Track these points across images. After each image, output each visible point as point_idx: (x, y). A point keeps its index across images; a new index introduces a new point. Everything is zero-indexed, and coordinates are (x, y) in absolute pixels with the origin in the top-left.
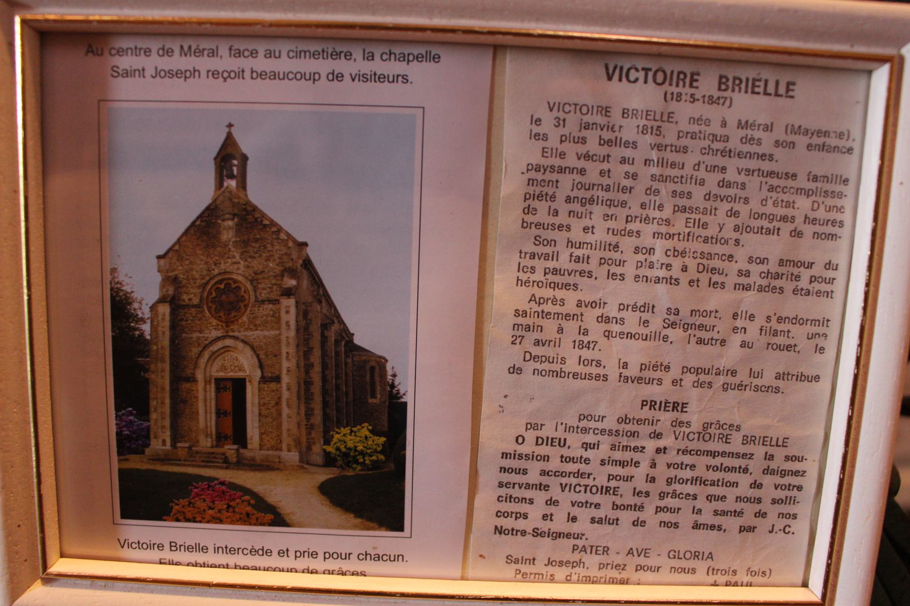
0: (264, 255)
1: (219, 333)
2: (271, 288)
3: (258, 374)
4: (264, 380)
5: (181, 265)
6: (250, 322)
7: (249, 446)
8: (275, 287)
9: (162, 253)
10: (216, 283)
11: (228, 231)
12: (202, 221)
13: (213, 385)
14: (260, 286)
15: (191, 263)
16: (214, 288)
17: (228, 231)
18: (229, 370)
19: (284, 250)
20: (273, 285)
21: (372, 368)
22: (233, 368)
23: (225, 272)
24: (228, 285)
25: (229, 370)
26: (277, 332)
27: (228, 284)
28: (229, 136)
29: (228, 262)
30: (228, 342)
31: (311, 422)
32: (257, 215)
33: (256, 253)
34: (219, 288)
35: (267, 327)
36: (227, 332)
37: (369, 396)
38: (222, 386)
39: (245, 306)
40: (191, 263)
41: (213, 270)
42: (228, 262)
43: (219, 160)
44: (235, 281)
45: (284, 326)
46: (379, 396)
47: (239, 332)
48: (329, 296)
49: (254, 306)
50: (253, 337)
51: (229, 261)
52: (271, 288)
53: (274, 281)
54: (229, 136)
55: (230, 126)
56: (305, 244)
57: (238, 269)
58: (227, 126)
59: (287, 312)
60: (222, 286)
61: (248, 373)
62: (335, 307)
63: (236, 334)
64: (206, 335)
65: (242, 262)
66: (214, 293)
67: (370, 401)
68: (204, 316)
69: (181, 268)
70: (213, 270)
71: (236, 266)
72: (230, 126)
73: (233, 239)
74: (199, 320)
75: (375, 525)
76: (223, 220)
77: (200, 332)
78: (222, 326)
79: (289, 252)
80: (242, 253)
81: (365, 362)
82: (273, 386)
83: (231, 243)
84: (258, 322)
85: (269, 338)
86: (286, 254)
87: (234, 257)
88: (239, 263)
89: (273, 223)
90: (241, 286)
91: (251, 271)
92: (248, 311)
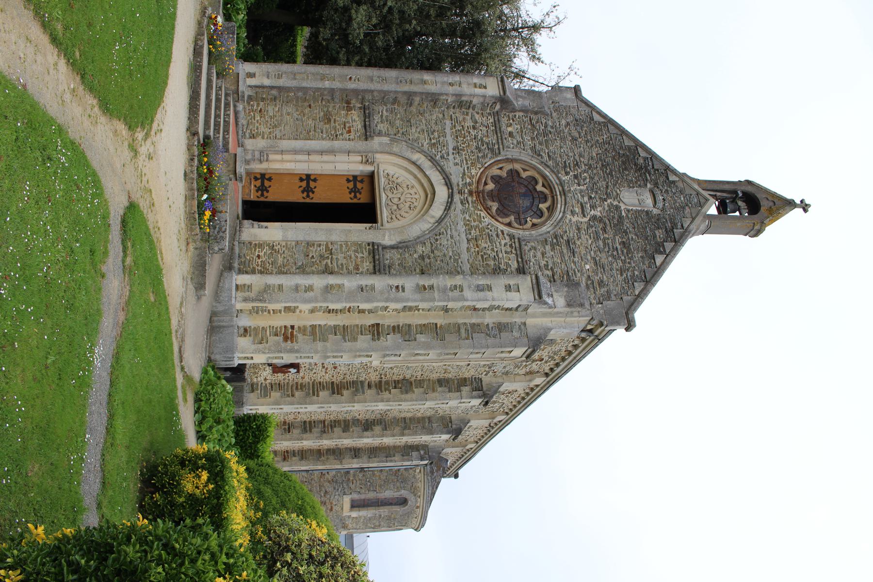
0: (603, 255)
1: (455, 179)
2: (546, 266)
3: (388, 241)
4: (375, 250)
5: (568, 124)
6: (482, 230)
7: (247, 223)
9: (586, 94)
10: (544, 177)
12: (645, 159)
15: (574, 139)
16: (537, 176)
18: (390, 196)
20: (552, 269)
21: (404, 502)
22: (395, 201)
23: (564, 193)
25: (390, 196)
26: (466, 267)
29: (583, 196)
30: (442, 193)
31: (300, 336)
32: (669, 246)
33: (605, 244)
34: (537, 183)
35: (476, 258)
37: (355, 496)
38: (359, 185)
40: (574, 139)
42: (583, 196)
43: (749, 189)
44: (551, 209)
45: (482, 281)
46: (354, 514)
49: (512, 237)
50: (455, 234)
51: (586, 199)
52: (546, 266)
53: (558, 270)
54: (790, 204)
55: (805, 207)
56: (630, 326)
58: (802, 201)
59: (508, 288)
60: (539, 188)
62: (507, 423)
64: (451, 157)
65: (586, 220)
66: (528, 174)
67: (347, 501)
68: (484, 157)
69: (563, 122)
70: (567, 173)
71: (577, 210)
72: (805, 207)
73: (623, 207)
74: (477, 148)
76: (652, 191)
78: (470, 184)
81: (414, 491)
82: (367, 265)
85: (456, 261)
86: (608, 292)
87: (593, 207)
88: (584, 216)
90: (543, 219)
91: (572, 234)
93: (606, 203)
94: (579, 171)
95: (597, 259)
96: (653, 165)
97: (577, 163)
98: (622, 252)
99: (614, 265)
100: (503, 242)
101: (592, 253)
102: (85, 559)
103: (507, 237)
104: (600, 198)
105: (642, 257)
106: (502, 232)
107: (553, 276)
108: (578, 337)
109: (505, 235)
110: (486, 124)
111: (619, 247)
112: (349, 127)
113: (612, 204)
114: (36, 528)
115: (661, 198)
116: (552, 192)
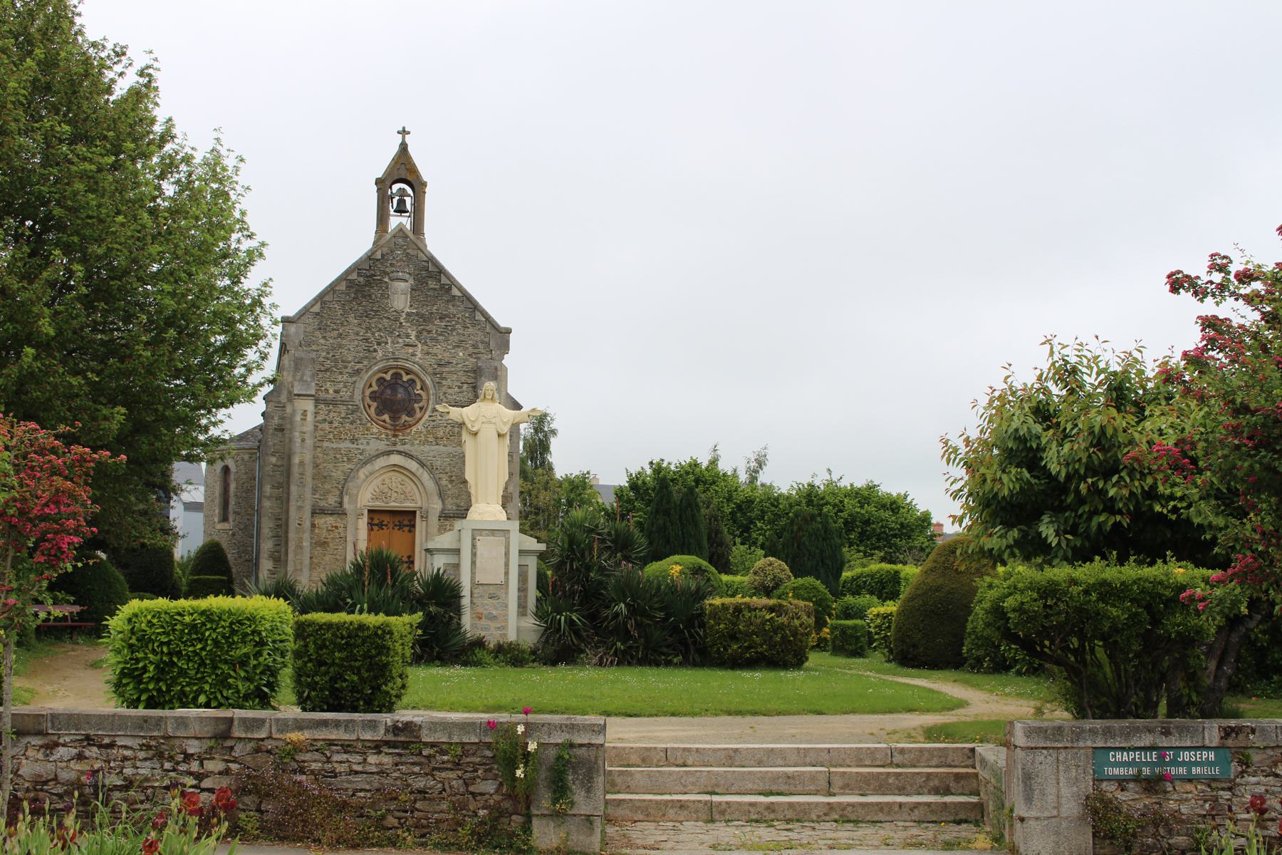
1: (382, 446)
2: (459, 387)
5: (324, 337)
8: (465, 386)
11: (400, 296)
12: (359, 275)
13: (366, 518)
14: (444, 382)
17: (400, 296)
19: (480, 336)
24: (397, 376)
27: (414, 381)
28: (404, 148)
36: (395, 444)
39: (371, 386)
41: (375, 351)
42: (398, 343)
47: (413, 444)
48: (321, 293)
51: (400, 340)
54: (404, 148)
57: (413, 355)
61: (419, 504)
63: (407, 448)
65: (419, 345)
69: (322, 341)
70: (375, 351)
72: (404, 132)
74: (352, 423)
75: (152, 596)
77: (354, 440)
78: (387, 435)
79: (487, 340)
80: (420, 332)
83: (404, 314)
84: (440, 434)
85: (454, 456)
87: (408, 336)
89: (467, 297)
92: (426, 417)
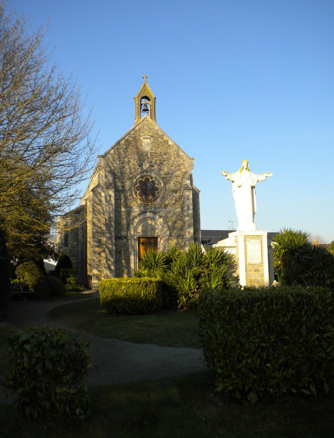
12: (129, 137)
93: (149, 157)
94: (136, 164)
95: (171, 165)
96: (132, 135)
97: (133, 164)
98: (168, 156)
99: (173, 160)
100: (166, 197)
101: (169, 167)
102: (31, 290)
103: (164, 195)
104: (147, 159)
105: (170, 149)
106: (162, 196)
107: (177, 182)
108: (42, 329)
109: (163, 195)
110: (119, 195)
111: (166, 157)
112: (123, 245)
113: (150, 155)
114: (331, 334)
115: (147, 136)
116: (145, 176)
